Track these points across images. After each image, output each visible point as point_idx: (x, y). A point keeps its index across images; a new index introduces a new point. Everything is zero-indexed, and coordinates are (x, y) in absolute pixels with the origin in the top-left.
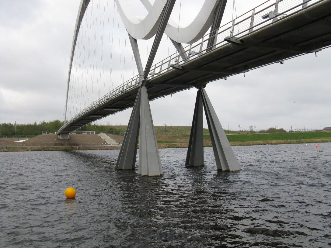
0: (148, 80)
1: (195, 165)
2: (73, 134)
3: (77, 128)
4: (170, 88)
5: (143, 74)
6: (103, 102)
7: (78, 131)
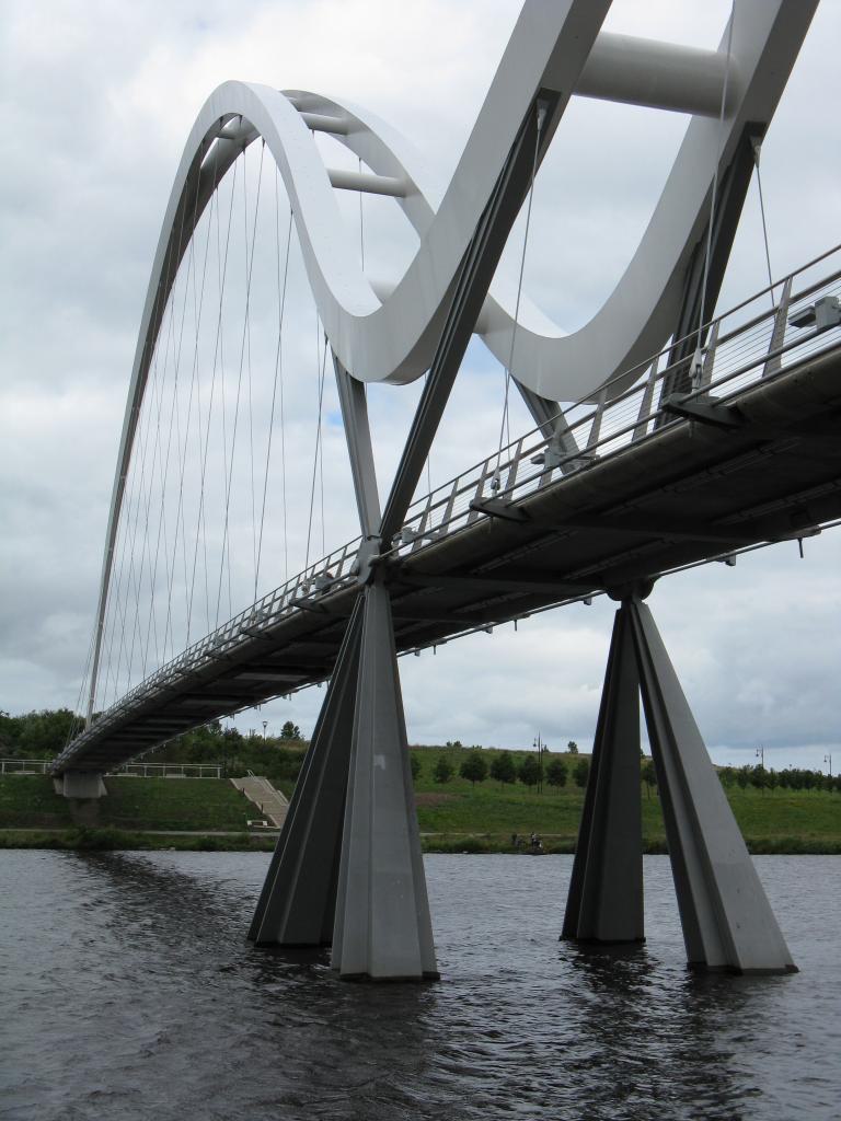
0: (394, 558)
1: (601, 936)
2: (129, 772)
3: (137, 750)
4: (500, 594)
5: (375, 529)
6: (271, 621)
7: (146, 766)
